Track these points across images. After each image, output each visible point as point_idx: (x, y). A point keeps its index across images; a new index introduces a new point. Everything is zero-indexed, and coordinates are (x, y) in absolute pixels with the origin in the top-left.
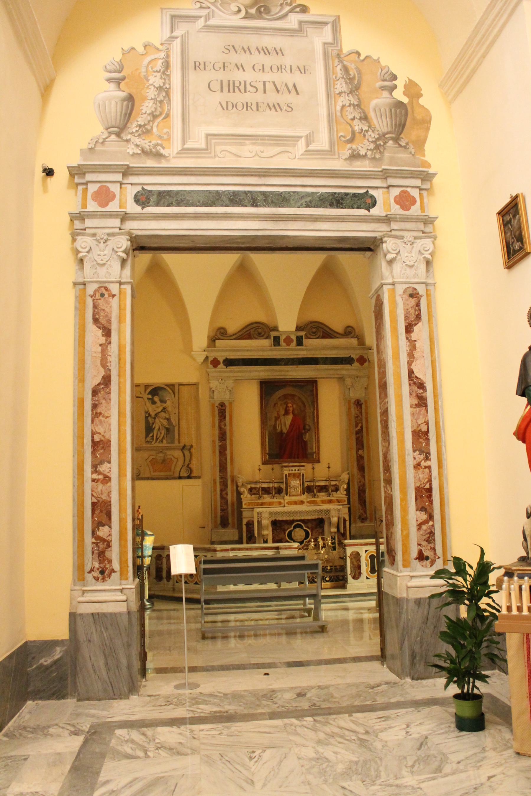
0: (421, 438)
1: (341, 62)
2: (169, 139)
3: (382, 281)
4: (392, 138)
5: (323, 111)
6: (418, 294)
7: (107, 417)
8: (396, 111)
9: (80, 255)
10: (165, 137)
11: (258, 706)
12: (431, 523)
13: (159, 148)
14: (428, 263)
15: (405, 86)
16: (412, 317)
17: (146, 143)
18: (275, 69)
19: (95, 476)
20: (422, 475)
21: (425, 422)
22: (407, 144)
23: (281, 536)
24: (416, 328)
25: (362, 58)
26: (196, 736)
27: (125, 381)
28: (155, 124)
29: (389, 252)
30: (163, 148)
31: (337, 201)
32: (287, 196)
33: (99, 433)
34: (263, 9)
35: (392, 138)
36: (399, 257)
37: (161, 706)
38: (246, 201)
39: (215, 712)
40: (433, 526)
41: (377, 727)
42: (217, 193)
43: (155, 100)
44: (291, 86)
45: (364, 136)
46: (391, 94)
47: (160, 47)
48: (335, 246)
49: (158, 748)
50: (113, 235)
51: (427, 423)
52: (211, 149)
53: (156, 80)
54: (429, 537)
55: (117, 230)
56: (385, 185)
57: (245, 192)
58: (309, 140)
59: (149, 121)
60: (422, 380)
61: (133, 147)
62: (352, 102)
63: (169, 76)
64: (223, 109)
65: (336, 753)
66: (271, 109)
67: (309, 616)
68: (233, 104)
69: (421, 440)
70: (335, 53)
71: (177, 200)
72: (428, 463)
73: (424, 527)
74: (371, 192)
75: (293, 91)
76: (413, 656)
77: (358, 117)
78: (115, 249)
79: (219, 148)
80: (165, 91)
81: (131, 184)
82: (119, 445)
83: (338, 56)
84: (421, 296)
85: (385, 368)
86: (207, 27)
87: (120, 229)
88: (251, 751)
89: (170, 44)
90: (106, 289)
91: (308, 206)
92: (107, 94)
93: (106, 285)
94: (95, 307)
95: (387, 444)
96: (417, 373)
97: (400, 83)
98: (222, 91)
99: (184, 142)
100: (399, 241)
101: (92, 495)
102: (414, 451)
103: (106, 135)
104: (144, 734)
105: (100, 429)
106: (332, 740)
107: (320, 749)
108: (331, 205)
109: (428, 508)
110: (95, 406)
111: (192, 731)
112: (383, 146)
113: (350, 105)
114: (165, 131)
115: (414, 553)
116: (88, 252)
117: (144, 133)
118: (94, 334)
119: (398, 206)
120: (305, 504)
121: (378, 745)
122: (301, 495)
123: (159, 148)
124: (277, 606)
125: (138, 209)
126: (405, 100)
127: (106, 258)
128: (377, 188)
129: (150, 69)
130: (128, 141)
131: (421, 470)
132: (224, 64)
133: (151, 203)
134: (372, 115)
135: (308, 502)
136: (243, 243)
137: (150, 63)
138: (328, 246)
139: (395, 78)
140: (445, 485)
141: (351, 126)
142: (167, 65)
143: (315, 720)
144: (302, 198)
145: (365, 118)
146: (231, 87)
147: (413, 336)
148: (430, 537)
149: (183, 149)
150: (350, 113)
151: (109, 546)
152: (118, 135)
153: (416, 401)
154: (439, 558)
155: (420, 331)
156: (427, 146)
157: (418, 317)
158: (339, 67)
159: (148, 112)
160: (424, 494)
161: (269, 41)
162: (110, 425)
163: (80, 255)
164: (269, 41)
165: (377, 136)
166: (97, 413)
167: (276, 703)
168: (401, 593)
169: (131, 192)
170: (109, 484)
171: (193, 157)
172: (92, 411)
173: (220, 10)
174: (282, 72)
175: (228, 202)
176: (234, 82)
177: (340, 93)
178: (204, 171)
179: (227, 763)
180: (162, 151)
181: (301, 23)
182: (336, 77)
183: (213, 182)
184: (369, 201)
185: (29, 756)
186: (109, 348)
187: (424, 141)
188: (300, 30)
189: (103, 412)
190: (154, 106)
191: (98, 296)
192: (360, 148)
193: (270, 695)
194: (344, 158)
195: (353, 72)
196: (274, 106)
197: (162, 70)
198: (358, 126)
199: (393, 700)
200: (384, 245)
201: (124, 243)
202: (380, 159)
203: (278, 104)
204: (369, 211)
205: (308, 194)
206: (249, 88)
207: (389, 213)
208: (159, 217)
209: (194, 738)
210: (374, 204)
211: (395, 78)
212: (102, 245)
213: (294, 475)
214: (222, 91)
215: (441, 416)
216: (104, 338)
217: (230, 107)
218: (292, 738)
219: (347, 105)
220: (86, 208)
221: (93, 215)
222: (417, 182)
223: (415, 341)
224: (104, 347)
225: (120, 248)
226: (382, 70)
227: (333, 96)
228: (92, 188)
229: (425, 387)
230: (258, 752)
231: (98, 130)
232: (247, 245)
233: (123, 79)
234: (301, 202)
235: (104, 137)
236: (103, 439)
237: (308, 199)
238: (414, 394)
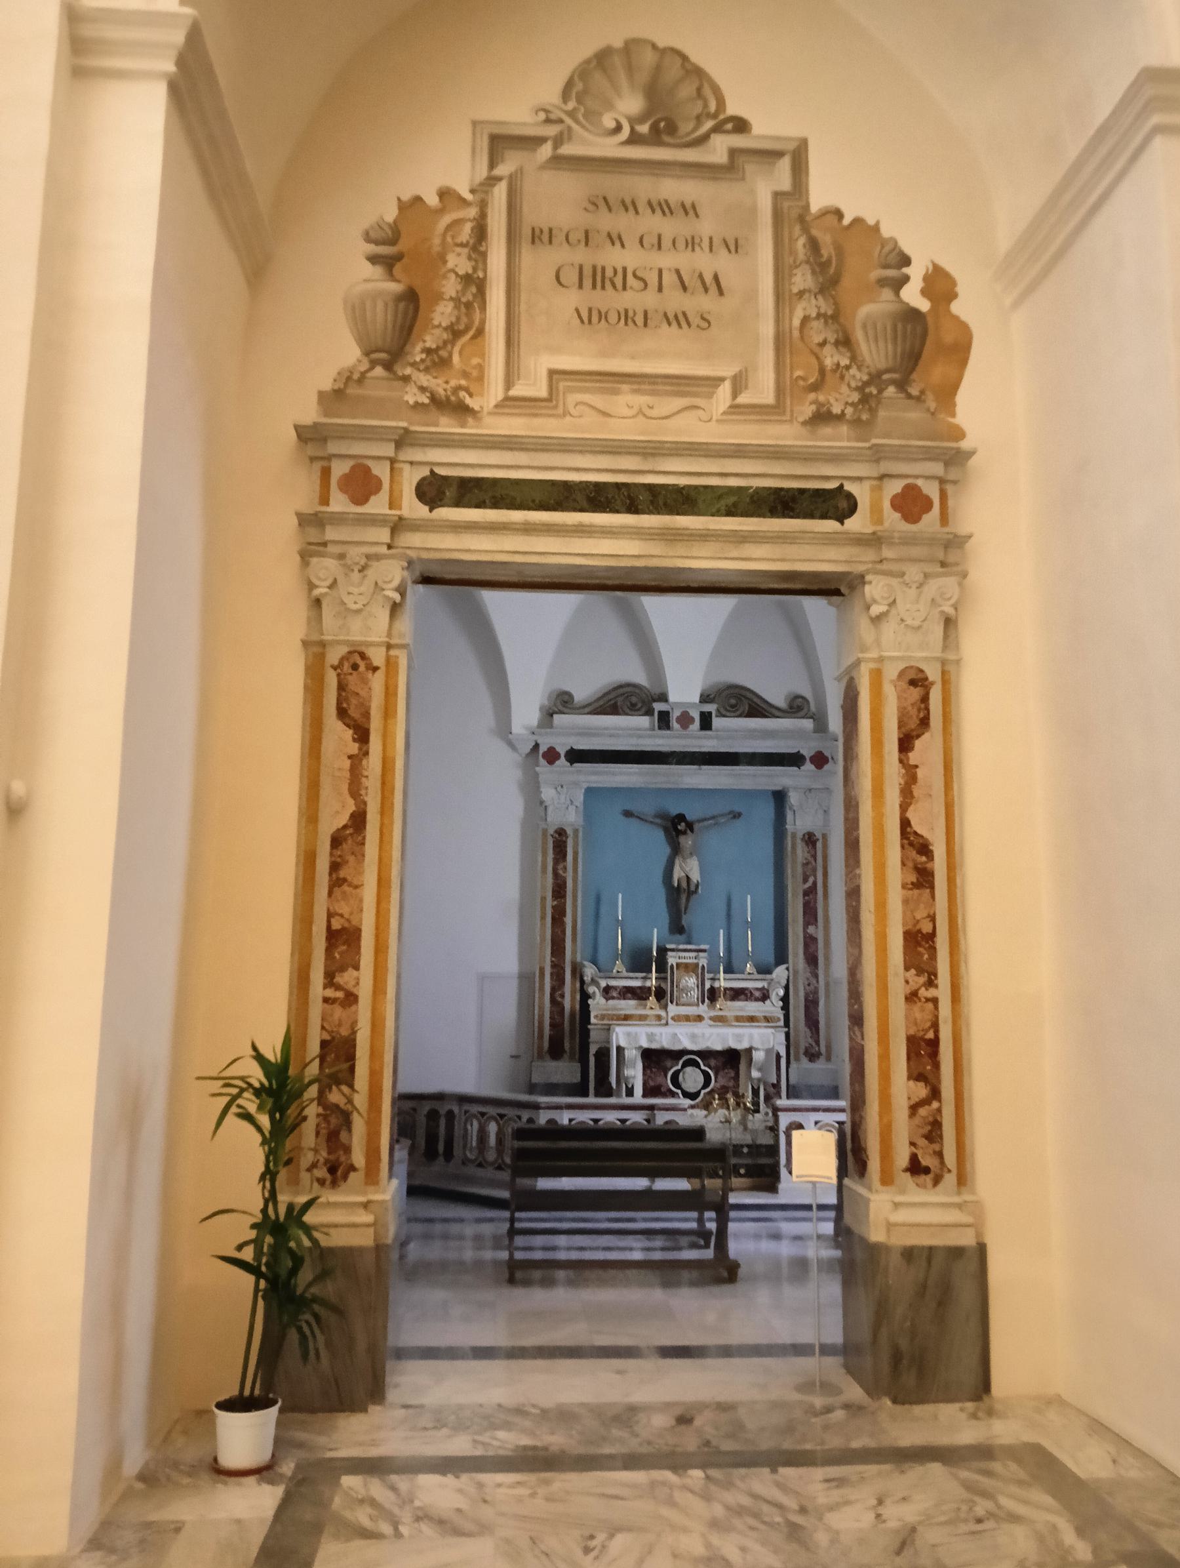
0: (921, 946)
1: (806, 230)
2: (481, 379)
3: (860, 655)
4: (893, 382)
5: (767, 329)
6: (927, 679)
7: (356, 887)
8: (905, 328)
9: (316, 592)
10: (475, 373)
11: (604, 1439)
12: (935, 1105)
13: (462, 394)
14: (949, 623)
15: (926, 278)
16: (913, 724)
17: (439, 384)
18: (681, 244)
19: (330, 993)
20: (922, 1014)
21: (929, 916)
22: (922, 392)
23: (660, 1080)
24: (918, 743)
25: (846, 221)
26: (488, 1498)
27: (392, 823)
28: (457, 349)
29: (875, 601)
30: (471, 395)
31: (783, 503)
32: (693, 493)
33: (342, 916)
34: (662, 124)
35: (893, 382)
36: (893, 612)
37: (425, 1429)
38: (618, 502)
39: (525, 1448)
40: (939, 1110)
41: (822, 1500)
42: (566, 485)
43: (456, 301)
44: (708, 279)
45: (842, 377)
46: (897, 293)
47: (469, 197)
48: (776, 586)
49: (418, 1519)
50: (378, 557)
51: (932, 918)
52: (557, 401)
53: (458, 262)
54: (930, 1132)
55: (384, 550)
56: (875, 475)
57: (618, 486)
58: (739, 383)
59: (445, 343)
60: (927, 840)
61: (415, 390)
62: (822, 311)
63: (484, 255)
64: (582, 322)
65: (743, 1549)
66: (669, 324)
67: (707, 1246)
68: (600, 312)
69: (921, 949)
70: (794, 213)
71: (494, 497)
72: (932, 992)
73: (923, 1111)
74: (848, 487)
75: (713, 289)
76: (897, 1357)
77: (832, 341)
78: (380, 583)
79: (573, 398)
80: (476, 284)
81: (411, 463)
82: (377, 936)
83: (802, 219)
84: (932, 683)
85: (857, 812)
86: (557, 161)
87: (390, 547)
88: (587, 1534)
89: (486, 192)
90: (363, 656)
91: (730, 513)
92: (370, 286)
93: (363, 649)
94: (341, 687)
95: (856, 952)
96: (917, 826)
97: (916, 272)
98: (581, 286)
99: (509, 384)
100: (894, 582)
101: (323, 1028)
102: (907, 969)
103: (365, 366)
104: (393, 1489)
105: (343, 908)
106: (737, 1522)
107: (715, 1540)
108: (773, 513)
109: (930, 1077)
110: (335, 867)
111: (480, 1486)
112: (876, 396)
113: (819, 316)
114: (475, 361)
115: (902, 1158)
116: (330, 587)
117: (434, 364)
118: (338, 736)
119: (898, 515)
120: (707, 1021)
121: (822, 1538)
122: (698, 1005)
123: (462, 394)
124: (645, 1220)
125: (422, 511)
126: (924, 305)
127: (363, 600)
128: (860, 479)
129: (449, 239)
130: (406, 379)
131: (919, 1004)
132: (587, 232)
133: (446, 500)
134: (859, 336)
135: (711, 1018)
136: (609, 579)
137: (449, 227)
138: (764, 586)
139: (906, 261)
140: (964, 1033)
141: (818, 358)
142: (481, 232)
143: (708, 1477)
144: (720, 497)
145: (845, 342)
146: (598, 278)
147: (913, 758)
148: (933, 1132)
149: (507, 398)
150: (818, 332)
151: (347, 1122)
152: (388, 366)
153: (913, 878)
154: (949, 1171)
155: (927, 749)
156: (963, 397)
157: (925, 722)
158: (801, 241)
159: (444, 325)
160: (924, 1051)
161: (672, 189)
162: (361, 901)
163: (316, 592)
164: (672, 189)
165: (865, 378)
166: (338, 879)
167: (637, 1436)
168: (876, 1235)
169: (410, 478)
170: (353, 1008)
171: (525, 415)
172: (330, 874)
173: (583, 127)
174: (693, 250)
175: (585, 504)
176: (603, 269)
177: (801, 294)
178: (543, 444)
179: (543, 1557)
180: (468, 401)
181: (733, 153)
182: (795, 262)
183: (559, 464)
184: (843, 504)
185: (183, 1523)
186: (364, 762)
187: (955, 387)
188: (732, 167)
189: (349, 878)
190: (456, 312)
191: (346, 667)
192: (832, 401)
193: (627, 1415)
194: (801, 419)
195: (827, 251)
196: (676, 317)
197: (472, 242)
198: (832, 357)
199: (856, 1444)
200: (867, 588)
201: (393, 573)
202: (870, 423)
203: (684, 314)
204: (842, 523)
205: (731, 490)
206: (631, 280)
207: (879, 528)
208: (460, 527)
209: (485, 1501)
210: (852, 508)
211: (906, 261)
212: (356, 576)
213: (687, 966)
214: (581, 286)
215: (959, 905)
216: (357, 745)
217: (595, 318)
218: (665, 1511)
219: (814, 315)
220: (328, 505)
221: (339, 519)
222: (937, 469)
223: (917, 766)
224: (356, 762)
225: (390, 582)
226: (883, 247)
227: (787, 298)
228: (339, 469)
229: (932, 851)
230: (601, 1537)
231: (347, 353)
232: (617, 582)
233: (399, 257)
234: (717, 506)
235: (362, 369)
236: (346, 925)
237: (731, 500)
238: (910, 864)
